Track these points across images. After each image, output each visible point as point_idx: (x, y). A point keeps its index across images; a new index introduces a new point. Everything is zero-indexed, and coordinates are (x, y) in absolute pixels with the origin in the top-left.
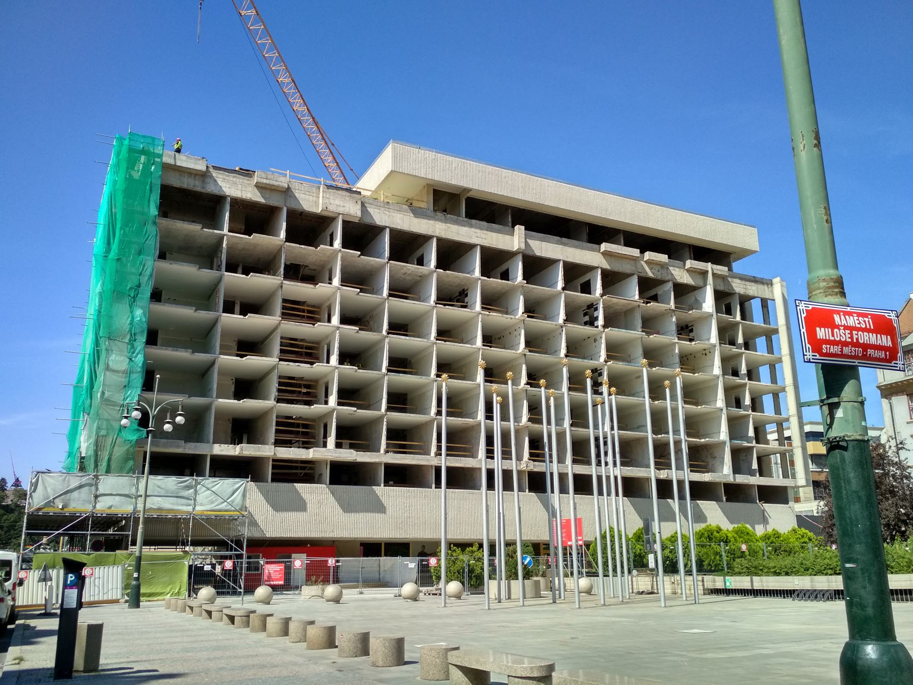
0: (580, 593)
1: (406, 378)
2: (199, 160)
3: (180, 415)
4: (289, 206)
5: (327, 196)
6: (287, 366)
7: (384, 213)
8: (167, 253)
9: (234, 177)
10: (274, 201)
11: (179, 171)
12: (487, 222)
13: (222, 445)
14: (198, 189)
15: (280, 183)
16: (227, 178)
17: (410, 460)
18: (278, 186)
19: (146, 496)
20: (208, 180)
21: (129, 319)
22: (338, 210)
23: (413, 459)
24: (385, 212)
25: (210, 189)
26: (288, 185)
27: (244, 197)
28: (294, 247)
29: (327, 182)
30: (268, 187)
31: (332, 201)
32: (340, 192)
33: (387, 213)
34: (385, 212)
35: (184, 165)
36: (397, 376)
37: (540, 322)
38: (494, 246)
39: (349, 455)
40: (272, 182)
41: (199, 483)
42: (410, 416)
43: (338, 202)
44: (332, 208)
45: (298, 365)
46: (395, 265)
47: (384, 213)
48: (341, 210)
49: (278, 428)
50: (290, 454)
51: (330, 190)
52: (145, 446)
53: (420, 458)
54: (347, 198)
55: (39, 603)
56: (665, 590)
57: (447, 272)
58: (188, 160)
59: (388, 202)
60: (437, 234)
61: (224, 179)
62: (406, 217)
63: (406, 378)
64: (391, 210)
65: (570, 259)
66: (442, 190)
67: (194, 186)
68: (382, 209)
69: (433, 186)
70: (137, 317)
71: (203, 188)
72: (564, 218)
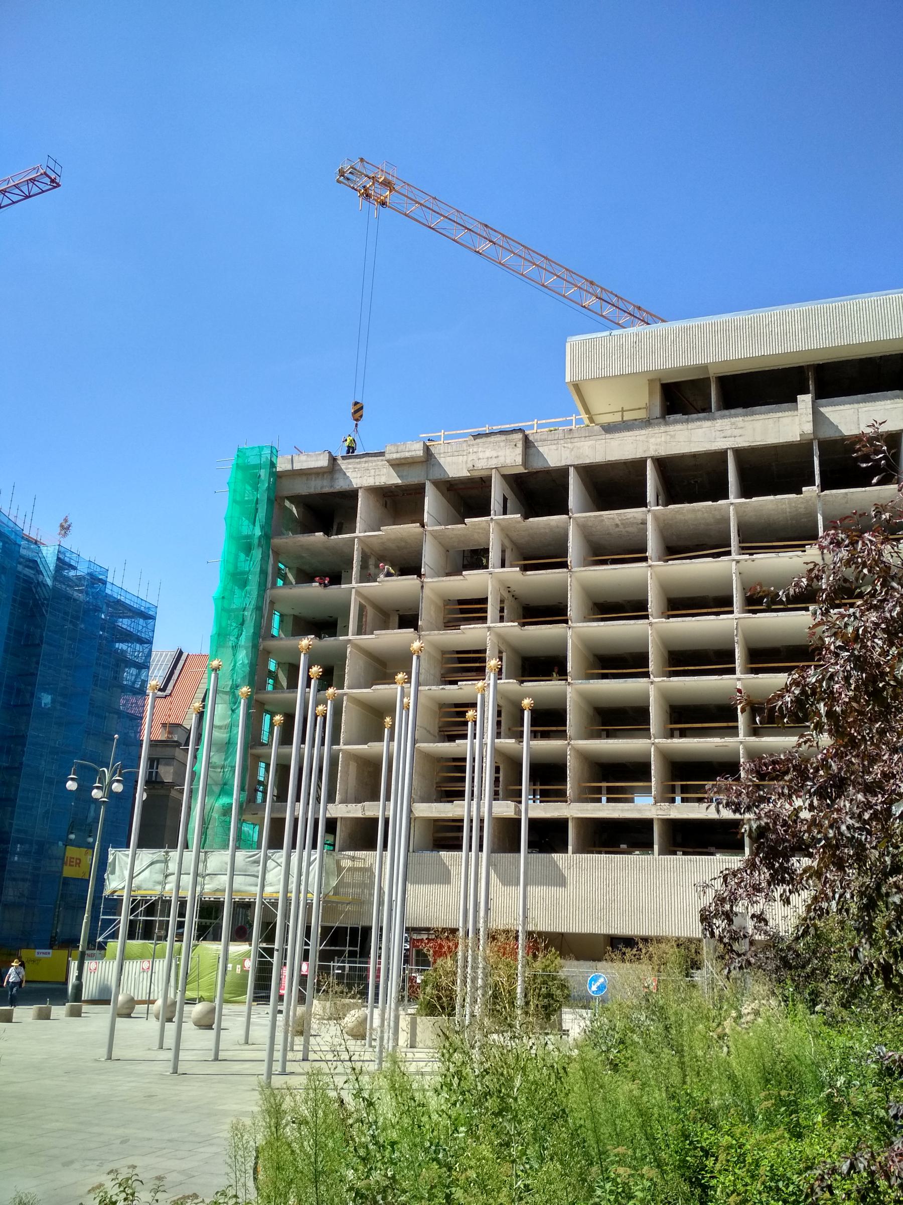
0: (247, 1043)
1: (601, 685)
2: (320, 454)
3: (72, 779)
4: (431, 478)
5: (475, 450)
6: (443, 691)
7: (564, 447)
8: (343, 571)
9: (366, 462)
10: (414, 477)
11: (306, 474)
12: (744, 408)
13: (349, 805)
14: (326, 490)
15: (413, 453)
16: (358, 466)
17: (607, 812)
18: (412, 458)
19: (180, 874)
20: (337, 476)
21: (232, 664)
22: (490, 464)
23: (614, 810)
24: (565, 445)
25: (340, 485)
26: (427, 449)
27: (377, 484)
28: (678, 512)
29: (494, 428)
30: (403, 461)
31: (481, 455)
32: (492, 439)
33: (569, 445)
34: (565, 445)
35: (305, 466)
36: (586, 684)
37: (762, 558)
38: (758, 444)
39: (605, 810)
40: (407, 455)
41: (270, 858)
42: (607, 743)
43: (489, 453)
44: (481, 464)
45: (443, 689)
46: (586, 517)
47: (564, 447)
48: (493, 463)
49: (463, 775)
50: (432, 812)
51: (478, 441)
52: (259, 813)
53: (626, 808)
54: (502, 444)
55: (144, 998)
56: (181, 1053)
57: (720, 502)
58: (309, 459)
59: (571, 430)
60: (652, 453)
61: (355, 468)
62: (599, 442)
63: (601, 685)
64: (576, 440)
65: (742, 442)
66: (683, 380)
67: (322, 488)
68: (562, 442)
69: (660, 380)
70: (239, 660)
71: (331, 486)
72: (867, 359)
